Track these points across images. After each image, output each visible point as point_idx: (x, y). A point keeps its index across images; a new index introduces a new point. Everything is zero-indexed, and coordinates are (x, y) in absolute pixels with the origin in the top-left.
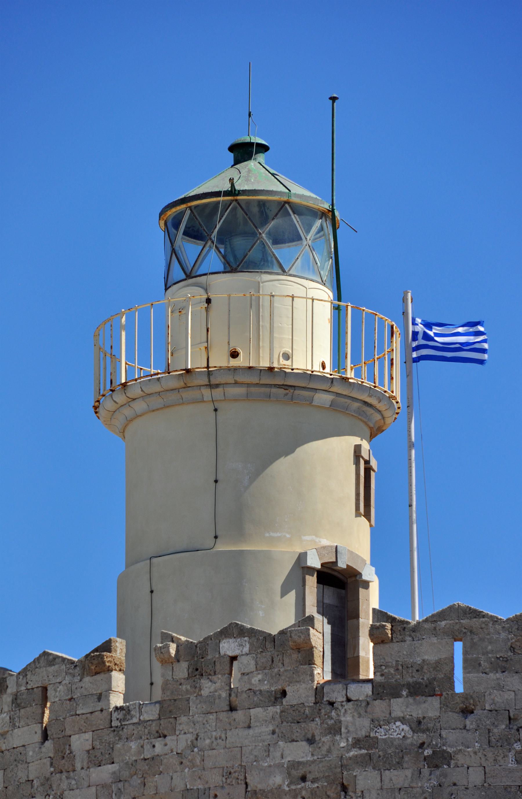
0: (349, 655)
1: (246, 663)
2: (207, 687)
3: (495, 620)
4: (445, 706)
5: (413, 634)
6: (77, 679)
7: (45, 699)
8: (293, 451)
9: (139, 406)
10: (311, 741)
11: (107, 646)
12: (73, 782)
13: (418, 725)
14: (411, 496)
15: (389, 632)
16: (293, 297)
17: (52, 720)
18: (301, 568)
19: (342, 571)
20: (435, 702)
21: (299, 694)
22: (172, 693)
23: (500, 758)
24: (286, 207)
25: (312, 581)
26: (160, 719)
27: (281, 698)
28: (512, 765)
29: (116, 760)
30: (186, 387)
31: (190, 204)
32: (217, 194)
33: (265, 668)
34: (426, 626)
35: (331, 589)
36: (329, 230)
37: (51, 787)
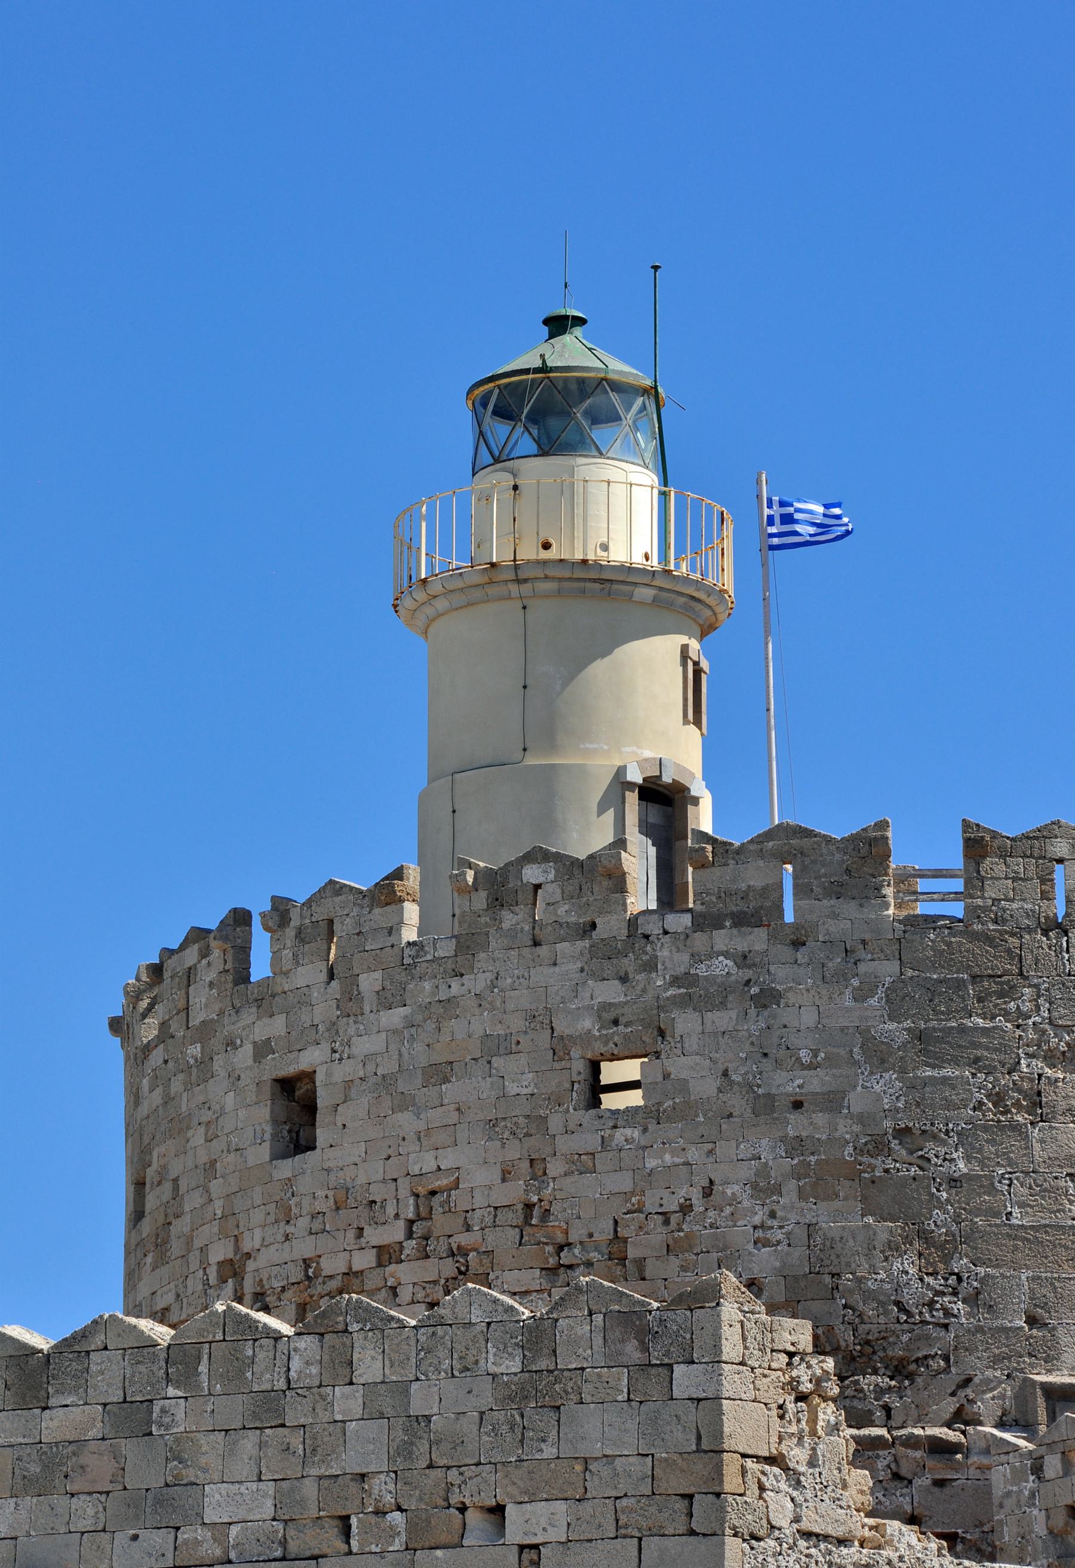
0: (677, 881)
1: (551, 892)
2: (508, 919)
3: (828, 840)
4: (772, 937)
5: (737, 857)
6: (366, 911)
7: (331, 933)
9: (441, 604)
10: (624, 979)
11: (398, 874)
12: (362, 1027)
13: (743, 960)
14: (768, 699)
15: (710, 855)
16: (609, 482)
17: (341, 956)
18: (620, 783)
19: (667, 786)
20: (762, 933)
21: (610, 926)
22: (470, 926)
23: (835, 996)
26: (456, 956)
27: (591, 931)
28: (849, 1003)
29: (408, 1002)
30: (491, 582)
31: (498, 383)
32: (526, 371)
33: (572, 897)
34: (752, 847)
35: (657, 806)
36: (651, 407)
37: (337, 1032)
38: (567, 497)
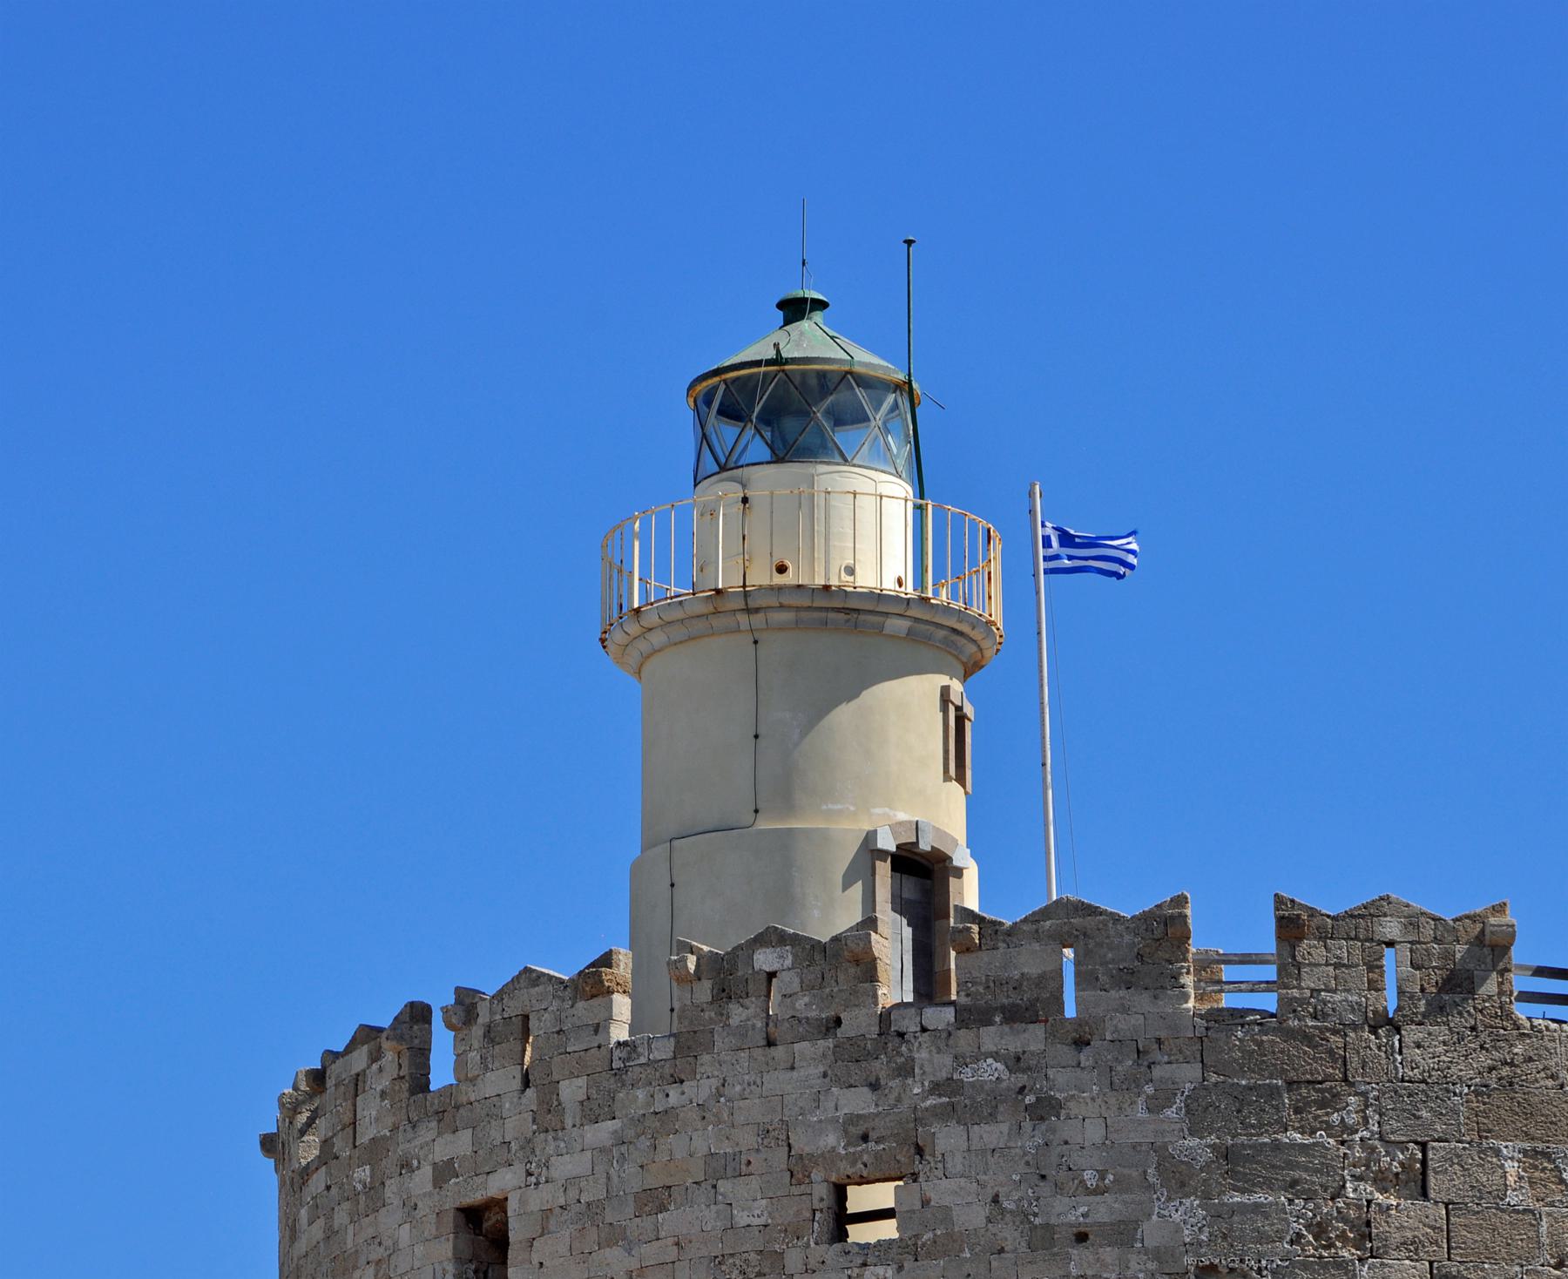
0: (937, 968)
2: (737, 1014)
3: (1116, 919)
4: (1051, 1035)
7: (526, 1032)
8: (857, 695)
9: (657, 638)
10: (875, 1086)
11: (606, 960)
13: (1016, 1062)
17: (538, 1059)
18: (869, 850)
19: (924, 855)
20: (1038, 1030)
21: (857, 1023)
22: (691, 1022)
24: (850, 378)
25: (884, 869)
28: (1141, 1114)
29: (617, 1114)
30: (716, 612)
32: (758, 363)
35: (913, 879)
36: (905, 405)
37: (533, 1151)
38: (807, 510)
